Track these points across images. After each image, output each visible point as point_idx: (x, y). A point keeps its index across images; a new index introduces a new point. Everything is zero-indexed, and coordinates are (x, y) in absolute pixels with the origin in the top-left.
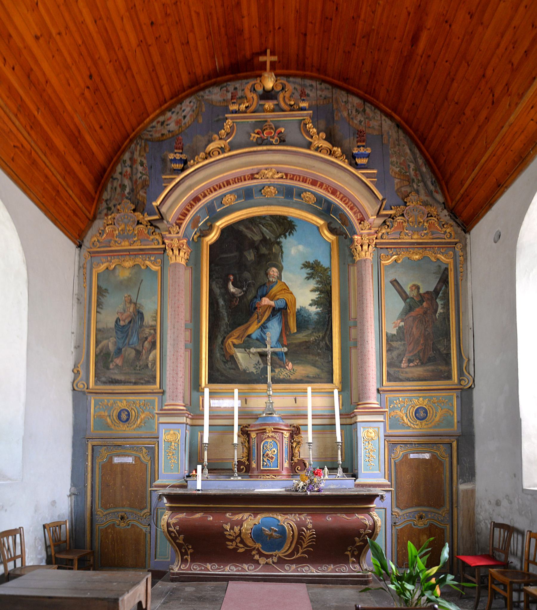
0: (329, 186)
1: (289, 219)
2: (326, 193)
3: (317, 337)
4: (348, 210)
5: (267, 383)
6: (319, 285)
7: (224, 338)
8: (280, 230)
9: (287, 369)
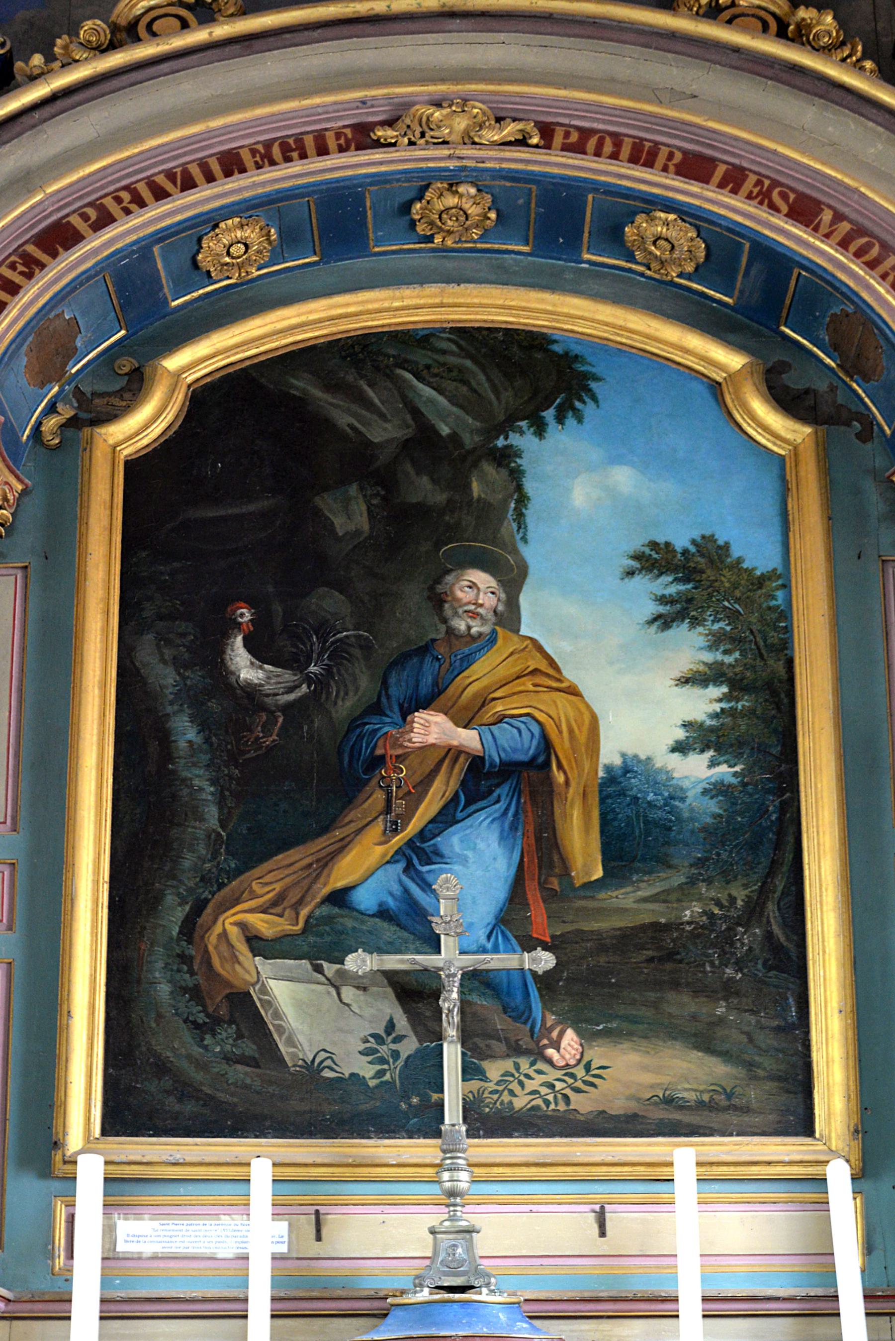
0: (775, 183)
1: (556, 348)
2: (763, 213)
3: (718, 904)
4: (881, 290)
5: (438, 1134)
6: (726, 652)
7: (199, 907)
8: (507, 395)
9: (550, 1062)
